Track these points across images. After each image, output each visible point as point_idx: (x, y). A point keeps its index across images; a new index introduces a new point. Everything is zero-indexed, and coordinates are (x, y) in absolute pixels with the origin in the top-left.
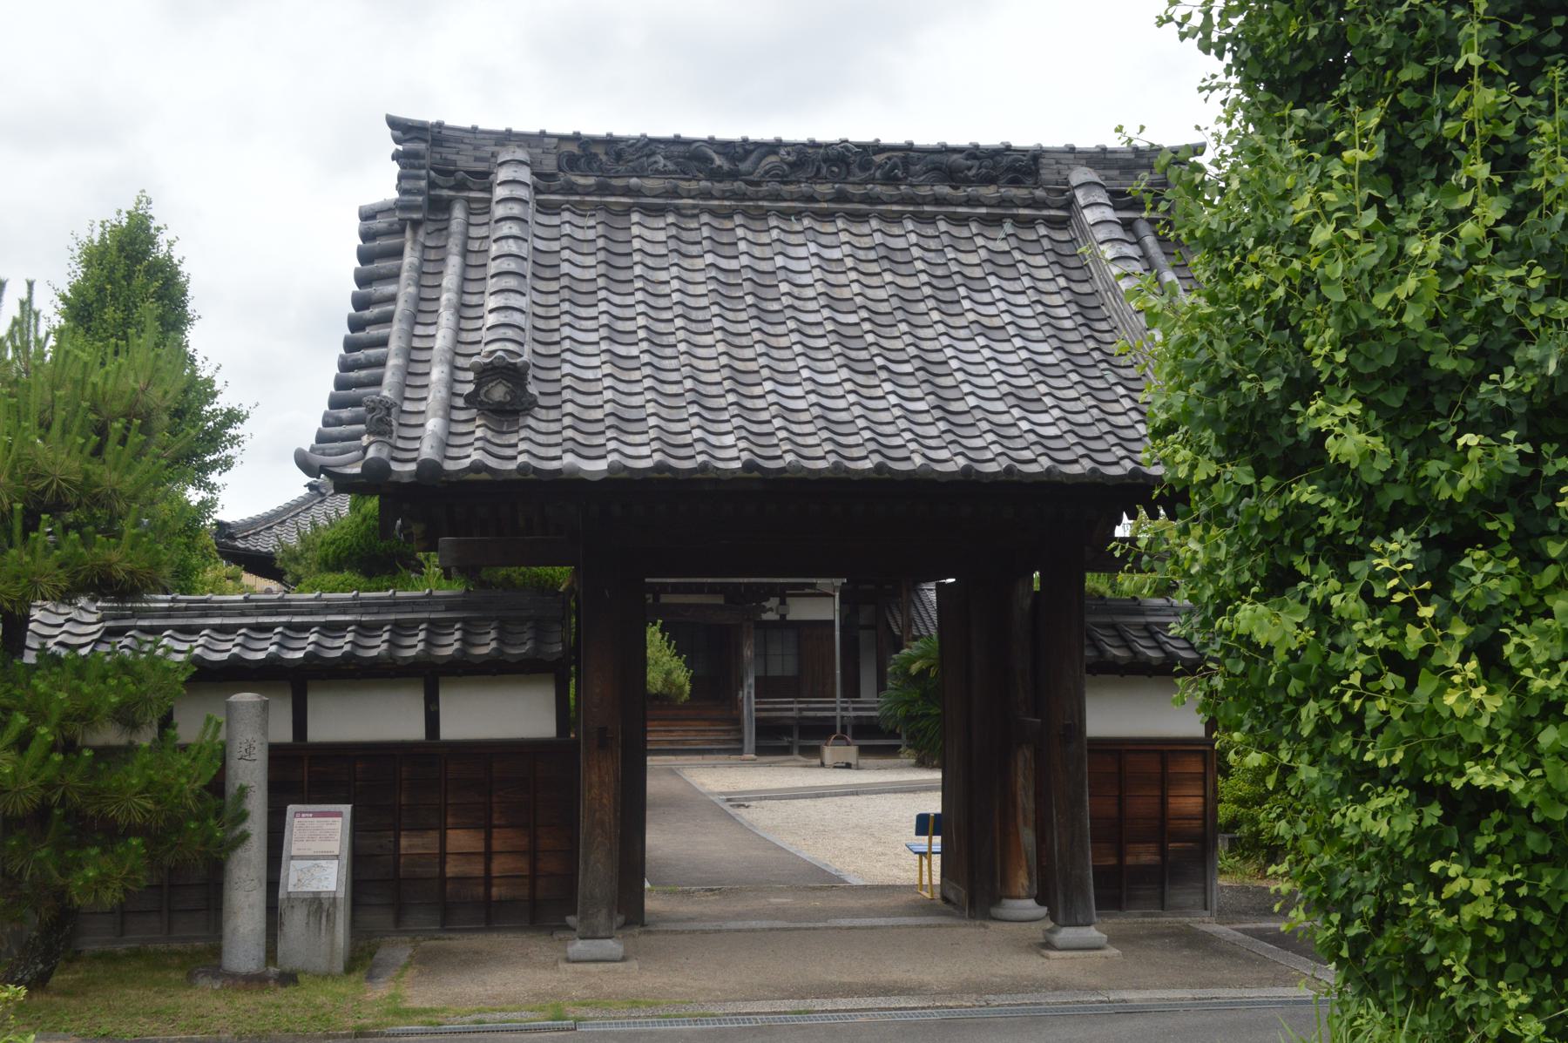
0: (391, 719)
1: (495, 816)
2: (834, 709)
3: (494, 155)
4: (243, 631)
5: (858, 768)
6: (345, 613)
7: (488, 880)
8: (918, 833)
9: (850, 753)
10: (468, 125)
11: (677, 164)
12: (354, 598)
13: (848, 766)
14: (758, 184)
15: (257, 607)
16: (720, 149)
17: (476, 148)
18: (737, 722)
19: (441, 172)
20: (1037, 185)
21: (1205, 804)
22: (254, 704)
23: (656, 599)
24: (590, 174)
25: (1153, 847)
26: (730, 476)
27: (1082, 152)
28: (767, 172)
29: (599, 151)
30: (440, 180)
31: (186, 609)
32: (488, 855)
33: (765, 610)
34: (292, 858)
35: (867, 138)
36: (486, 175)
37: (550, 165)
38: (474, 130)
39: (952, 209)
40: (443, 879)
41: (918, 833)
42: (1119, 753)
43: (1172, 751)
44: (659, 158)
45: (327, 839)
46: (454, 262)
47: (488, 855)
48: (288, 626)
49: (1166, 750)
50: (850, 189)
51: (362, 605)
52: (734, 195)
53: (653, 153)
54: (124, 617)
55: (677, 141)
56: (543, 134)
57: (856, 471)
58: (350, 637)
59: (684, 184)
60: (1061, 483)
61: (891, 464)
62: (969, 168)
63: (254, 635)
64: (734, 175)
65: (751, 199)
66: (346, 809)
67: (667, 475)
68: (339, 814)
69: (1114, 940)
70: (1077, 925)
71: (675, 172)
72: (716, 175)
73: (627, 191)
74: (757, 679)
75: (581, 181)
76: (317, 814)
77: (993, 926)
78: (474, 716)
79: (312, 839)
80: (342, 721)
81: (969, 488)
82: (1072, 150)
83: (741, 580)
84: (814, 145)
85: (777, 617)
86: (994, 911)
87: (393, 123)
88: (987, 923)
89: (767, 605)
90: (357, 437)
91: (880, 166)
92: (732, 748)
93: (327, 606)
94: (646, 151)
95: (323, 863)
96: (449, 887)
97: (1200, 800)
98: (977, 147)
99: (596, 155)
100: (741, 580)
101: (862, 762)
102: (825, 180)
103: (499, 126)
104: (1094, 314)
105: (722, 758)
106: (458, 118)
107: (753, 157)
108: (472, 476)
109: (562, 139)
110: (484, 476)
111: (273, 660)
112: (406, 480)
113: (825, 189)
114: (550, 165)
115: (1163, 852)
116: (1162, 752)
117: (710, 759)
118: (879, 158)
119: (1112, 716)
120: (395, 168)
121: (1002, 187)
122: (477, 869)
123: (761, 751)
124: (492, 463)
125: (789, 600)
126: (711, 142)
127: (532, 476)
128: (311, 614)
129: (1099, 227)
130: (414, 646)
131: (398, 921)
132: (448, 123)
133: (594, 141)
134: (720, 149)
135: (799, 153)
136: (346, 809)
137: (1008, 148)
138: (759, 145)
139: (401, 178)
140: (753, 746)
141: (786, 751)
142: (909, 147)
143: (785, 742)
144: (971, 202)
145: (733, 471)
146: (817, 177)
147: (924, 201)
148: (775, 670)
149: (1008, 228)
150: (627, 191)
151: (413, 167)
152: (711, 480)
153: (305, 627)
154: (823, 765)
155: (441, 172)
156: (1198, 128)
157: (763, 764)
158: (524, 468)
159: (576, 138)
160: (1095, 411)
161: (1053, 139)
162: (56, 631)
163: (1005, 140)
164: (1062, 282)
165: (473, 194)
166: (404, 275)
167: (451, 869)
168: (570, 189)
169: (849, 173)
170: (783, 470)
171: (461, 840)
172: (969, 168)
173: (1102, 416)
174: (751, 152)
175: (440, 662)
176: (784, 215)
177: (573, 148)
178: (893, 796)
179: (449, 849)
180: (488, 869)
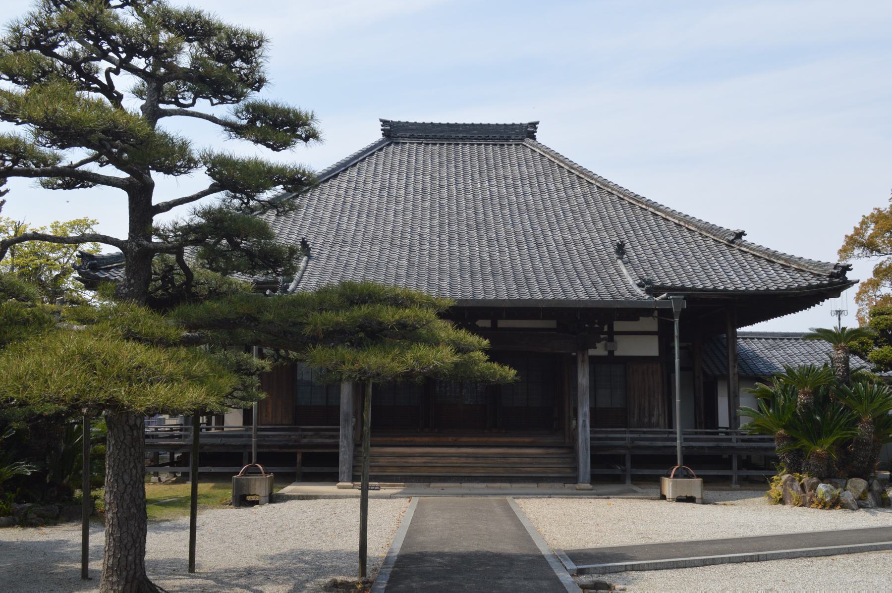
2: (772, 440)
5: (704, 502)
9: (694, 486)
13: (691, 500)
18: (572, 449)
85: (605, 353)
87: (381, 120)
101: (710, 494)
105: (558, 485)
117: (545, 487)
123: (596, 479)
125: (616, 338)
140: (588, 476)
141: (617, 479)
143: (618, 470)
154: (663, 497)
156: (621, 249)
157: (599, 495)
178: (805, 562)
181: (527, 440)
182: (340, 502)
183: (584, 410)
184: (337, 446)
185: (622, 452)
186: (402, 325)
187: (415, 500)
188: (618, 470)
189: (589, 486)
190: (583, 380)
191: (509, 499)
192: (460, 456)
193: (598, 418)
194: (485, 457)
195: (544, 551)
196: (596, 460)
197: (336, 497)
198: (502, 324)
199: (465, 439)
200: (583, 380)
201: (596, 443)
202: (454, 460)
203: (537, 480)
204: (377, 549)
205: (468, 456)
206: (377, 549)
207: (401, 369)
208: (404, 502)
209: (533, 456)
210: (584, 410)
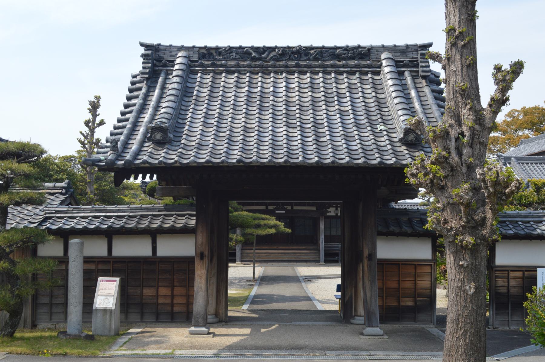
0: (140, 248)
1: (175, 283)
3: (176, 55)
4: (90, 218)
6: (124, 212)
7: (172, 305)
8: (337, 291)
10: (168, 44)
11: (240, 56)
12: (153, 206)
14: (268, 62)
15: (96, 210)
16: (255, 50)
17: (170, 52)
19: (157, 60)
20: (369, 60)
21: (431, 284)
22: (77, 243)
23: (292, 208)
24: (208, 59)
25: (411, 299)
26: (232, 165)
27: (387, 47)
28: (271, 58)
29: (213, 52)
30: (158, 64)
31: (72, 210)
32: (173, 296)
33: (328, 212)
34: (98, 295)
35: (307, 44)
36: (173, 61)
37: (195, 57)
38: (171, 46)
39: (374, 69)
40: (157, 304)
41: (337, 291)
42: (385, 264)
43: (418, 264)
44: (234, 54)
45: (110, 289)
46: (157, 91)
47: (173, 296)
48: (105, 216)
49: (416, 264)
50: (301, 63)
51: (130, 209)
52: (259, 66)
53: (232, 52)
54: (52, 213)
55: (241, 48)
56: (194, 47)
57: (278, 163)
58: (124, 220)
59: (242, 63)
60: (353, 167)
61: (337, 160)
62: (345, 54)
63: (105, 219)
64: (260, 59)
65: (265, 67)
66: (118, 279)
67: (210, 164)
68: (115, 281)
69: (386, 333)
70: (372, 327)
71: (239, 58)
72: (254, 59)
73: (222, 66)
74: (325, 236)
75: (206, 63)
76: (108, 281)
77: (350, 326)
78: (168, 248)
79: (105, 289)
80: (125, 249)
81: (320, 169)
82: (383, 46)
83: (266, 201)
84: (289, 47)
85: (334, 214)
86: (352, 321)
88: (348, 325)
89: (329, 210)
90: (107, 152)
91: (312, 54)
92: (316, 261)
93: (119, 210)
94: (229, 51)
95: (108, 297)
96: (159, 307)
97: (429, 282)
98: (348, 46)
99: (212, 53)
100: (266, 201)
102: (292, 60)
103: (179, 44)
104: (383, 105)
106: (165, 42)
107: (267, 53)
108: (143, 165)
109: (200, 48)
110: (147, 165)
111: (122, 227)
112: (121, 167)
113: (293, 63)
114: (195, 57)
115: (415, 302)
116: (415, 264)
117: (308, 264)
118: (312, 52)
119: (388, 250)
120: (141, 60)
121: (358, 60)
122: (168, 301)
124: (151, 161)
126: (252, 48)
127: (163, 165)
128: (113, 212)
129: (389, 74)
130: (144, 224)
131: (142, 318)
132: (162, 44)
133: (211, 48)
134: (255, 50)
135: (283, 51)
136: (118, 279)
137: (359, 47)
138: (269, 48)
139: (143, 63)
142: (323, 47)
143: (336, 258)
144: (344, 66)
145: (233, 163)
146: (290, 59)
147: (327, 66)
148: (334, 233)
149: (357, 75)
150: (222, 66)
151: (147, 59)
152: (227, 166)
153: (111, 217)
155: (157, 60)
158: (161, 162)
159: (205, 47)
160: (373, 141)
161: (376, 42)
162: (29, 218)
163: (394, 43)
164: (374, 94)
165: (168, 68)
166: (140, 96)
167: (161, 301)
168: (202, 65)
169: (301, 57)
170: (251, 162)
171: (163, 291)
172: (345, 54)
173: (375, 142)
174: (266, 51)
175: (153, 229)
176: (276, 73)
177: (204, 51)
179: (160, 293)
180: (172, 301)
181: (304, 247)
182: (239, 268)
183: (322, 237)
184: (235, 250)
185: (338, 252)
186: (265, 225)
187: (263, 268)
188: (336, 258)
189: (324, 263)
190: (322, 226)
191: (295, 268)
192: (279, 253)
193: (328, 239)
194: (288, 253)
195: (299, 275)
196: (326, 255)
197: (237, 267)
198: (295, 208)
199: (281, 247)
200: (322, 226)
201: (234, 258)
202: (277, 255)
203: (306, 261)
204: (256, 276)
205: (281, 253)
206: (256, 276)
207: (265, 234)
208: (260, 268)
209: (305, 253)
210: (322, 237)
